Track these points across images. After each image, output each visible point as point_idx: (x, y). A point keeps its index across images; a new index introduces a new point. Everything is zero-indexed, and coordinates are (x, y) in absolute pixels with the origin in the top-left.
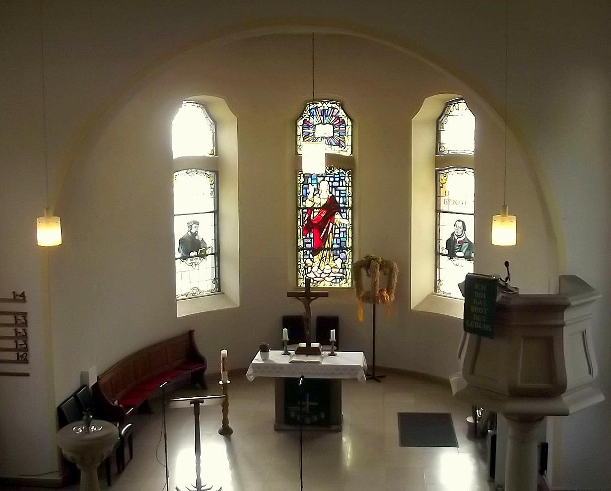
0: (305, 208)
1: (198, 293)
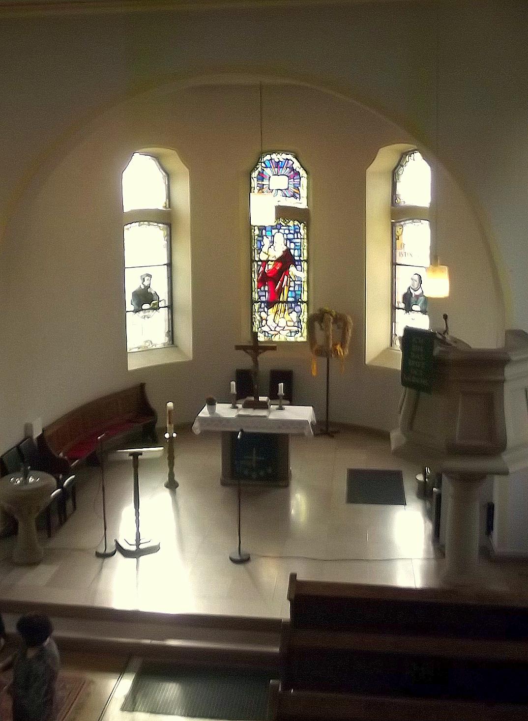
0: (260, 260)
1: (151, 346)
